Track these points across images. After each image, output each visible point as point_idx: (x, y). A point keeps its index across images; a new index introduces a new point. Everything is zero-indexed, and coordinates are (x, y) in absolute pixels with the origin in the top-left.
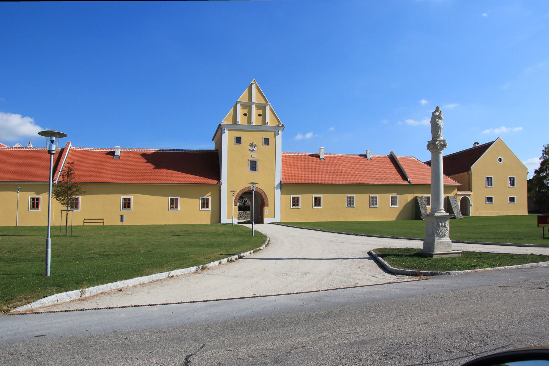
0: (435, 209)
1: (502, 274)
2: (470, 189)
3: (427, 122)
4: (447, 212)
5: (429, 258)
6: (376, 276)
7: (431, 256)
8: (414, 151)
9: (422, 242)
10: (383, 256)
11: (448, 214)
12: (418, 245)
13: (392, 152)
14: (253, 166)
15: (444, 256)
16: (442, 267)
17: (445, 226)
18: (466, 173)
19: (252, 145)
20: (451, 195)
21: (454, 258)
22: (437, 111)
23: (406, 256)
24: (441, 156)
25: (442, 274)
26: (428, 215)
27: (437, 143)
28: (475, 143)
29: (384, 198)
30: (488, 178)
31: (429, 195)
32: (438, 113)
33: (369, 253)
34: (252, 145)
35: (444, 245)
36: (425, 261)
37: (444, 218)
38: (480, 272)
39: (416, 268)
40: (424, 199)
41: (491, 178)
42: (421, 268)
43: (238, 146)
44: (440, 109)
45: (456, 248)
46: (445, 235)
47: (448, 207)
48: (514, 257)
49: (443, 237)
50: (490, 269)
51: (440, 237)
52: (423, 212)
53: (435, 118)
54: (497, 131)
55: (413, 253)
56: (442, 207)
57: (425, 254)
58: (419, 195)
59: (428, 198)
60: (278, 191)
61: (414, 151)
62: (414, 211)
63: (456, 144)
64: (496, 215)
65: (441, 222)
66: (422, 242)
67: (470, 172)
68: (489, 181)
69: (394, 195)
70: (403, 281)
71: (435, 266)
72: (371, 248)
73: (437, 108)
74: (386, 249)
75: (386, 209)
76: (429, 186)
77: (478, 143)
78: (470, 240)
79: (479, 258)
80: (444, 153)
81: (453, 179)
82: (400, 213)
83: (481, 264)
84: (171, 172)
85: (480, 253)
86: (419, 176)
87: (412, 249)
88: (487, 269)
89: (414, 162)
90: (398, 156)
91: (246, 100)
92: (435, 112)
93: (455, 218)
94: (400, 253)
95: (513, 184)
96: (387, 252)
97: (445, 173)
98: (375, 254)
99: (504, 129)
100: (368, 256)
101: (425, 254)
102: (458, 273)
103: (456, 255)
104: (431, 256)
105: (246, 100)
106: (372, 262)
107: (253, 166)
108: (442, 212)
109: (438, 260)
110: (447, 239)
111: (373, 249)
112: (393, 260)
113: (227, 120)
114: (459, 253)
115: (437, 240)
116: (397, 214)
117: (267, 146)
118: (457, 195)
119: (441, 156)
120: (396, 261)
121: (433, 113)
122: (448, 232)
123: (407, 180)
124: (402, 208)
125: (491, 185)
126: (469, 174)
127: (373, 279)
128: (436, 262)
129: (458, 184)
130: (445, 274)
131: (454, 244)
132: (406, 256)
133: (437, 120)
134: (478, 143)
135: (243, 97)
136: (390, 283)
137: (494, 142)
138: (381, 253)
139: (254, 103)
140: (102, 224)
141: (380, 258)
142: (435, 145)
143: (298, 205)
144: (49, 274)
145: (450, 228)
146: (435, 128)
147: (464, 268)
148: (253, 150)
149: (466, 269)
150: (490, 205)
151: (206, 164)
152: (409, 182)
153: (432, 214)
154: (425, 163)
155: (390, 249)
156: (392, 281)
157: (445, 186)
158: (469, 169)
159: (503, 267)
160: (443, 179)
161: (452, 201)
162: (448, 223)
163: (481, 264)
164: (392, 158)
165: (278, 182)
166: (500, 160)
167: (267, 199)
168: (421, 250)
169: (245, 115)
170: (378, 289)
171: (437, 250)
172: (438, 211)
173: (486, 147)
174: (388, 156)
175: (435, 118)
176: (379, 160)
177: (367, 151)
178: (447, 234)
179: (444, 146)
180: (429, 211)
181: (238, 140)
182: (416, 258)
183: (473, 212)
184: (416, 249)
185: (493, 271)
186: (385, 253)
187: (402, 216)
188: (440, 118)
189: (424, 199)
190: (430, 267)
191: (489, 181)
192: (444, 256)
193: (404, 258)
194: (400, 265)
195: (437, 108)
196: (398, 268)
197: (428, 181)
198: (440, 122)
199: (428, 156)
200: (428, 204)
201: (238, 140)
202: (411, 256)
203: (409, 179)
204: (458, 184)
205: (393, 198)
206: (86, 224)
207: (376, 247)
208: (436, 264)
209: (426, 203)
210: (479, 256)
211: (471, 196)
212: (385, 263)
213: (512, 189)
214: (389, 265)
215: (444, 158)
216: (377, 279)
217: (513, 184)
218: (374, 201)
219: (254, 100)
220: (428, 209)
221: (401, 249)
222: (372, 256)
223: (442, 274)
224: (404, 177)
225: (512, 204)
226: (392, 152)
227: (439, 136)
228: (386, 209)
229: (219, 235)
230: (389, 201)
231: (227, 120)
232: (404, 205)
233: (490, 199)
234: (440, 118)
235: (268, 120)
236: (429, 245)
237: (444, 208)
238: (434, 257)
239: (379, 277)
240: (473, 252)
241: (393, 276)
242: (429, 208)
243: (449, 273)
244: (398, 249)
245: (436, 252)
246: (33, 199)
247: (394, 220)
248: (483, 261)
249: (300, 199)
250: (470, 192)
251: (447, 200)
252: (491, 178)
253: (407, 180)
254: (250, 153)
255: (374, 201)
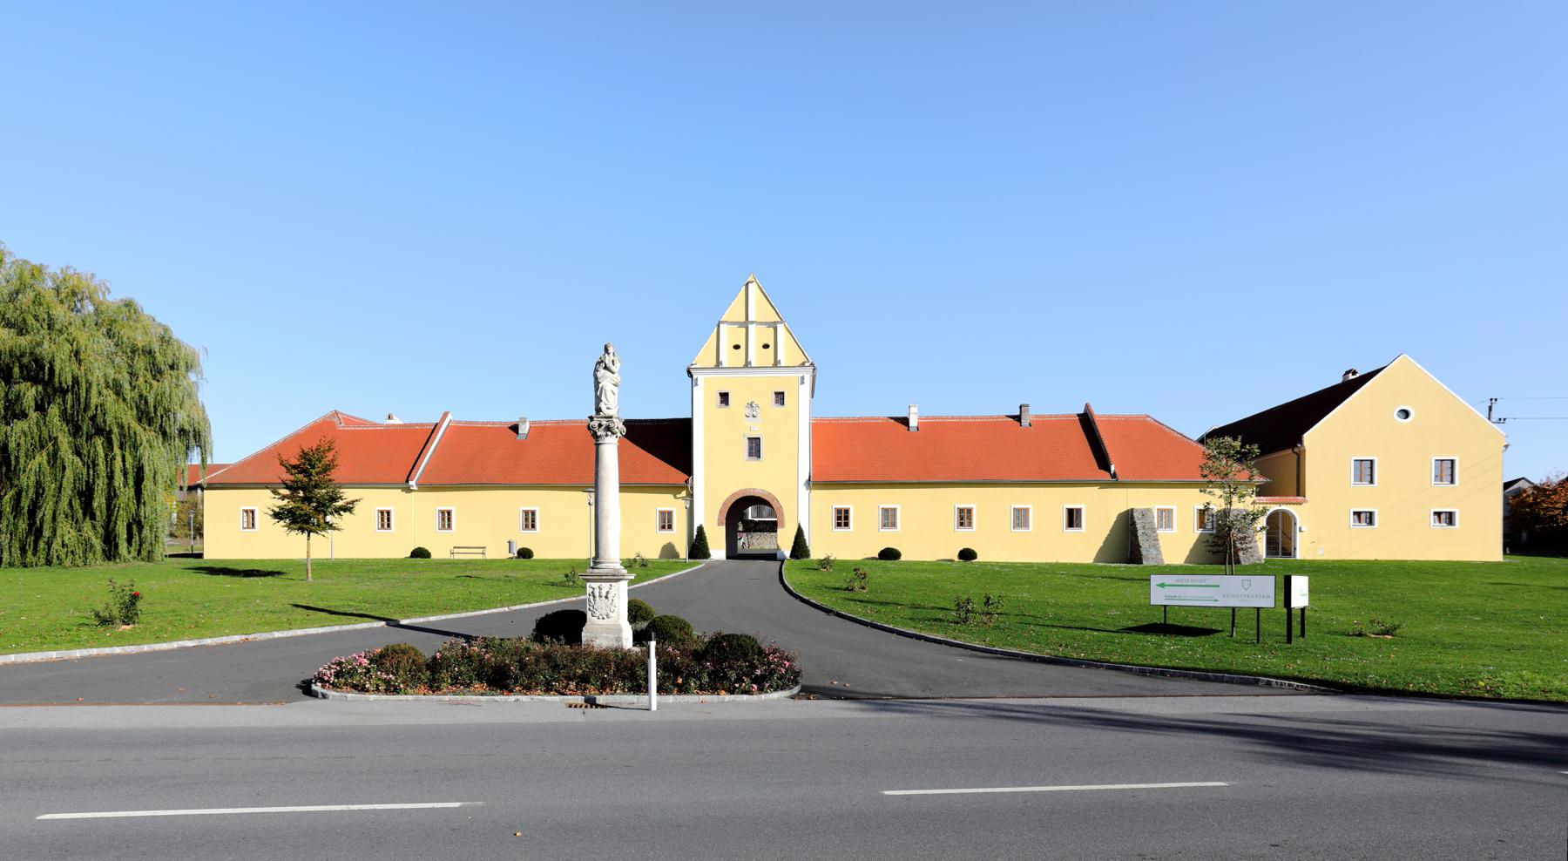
14: (755, 447)
43: (724, 409)
68: (1366, 470)
77: (1354, 373)
84: (38, 708)
90: (1098, 412)
107: (755, 447)
113: (705, 357)
135: (735, 311)
140: (480, 557)
143: (847, 525)
151: (666, 442)
158: (1300, 441)
164: (1086, 420)
176: (1050, 426)
191: (1366, 470)
203: (1113, 468)
206: (457, 557)
231: (705, 357)
249: (974, 513)
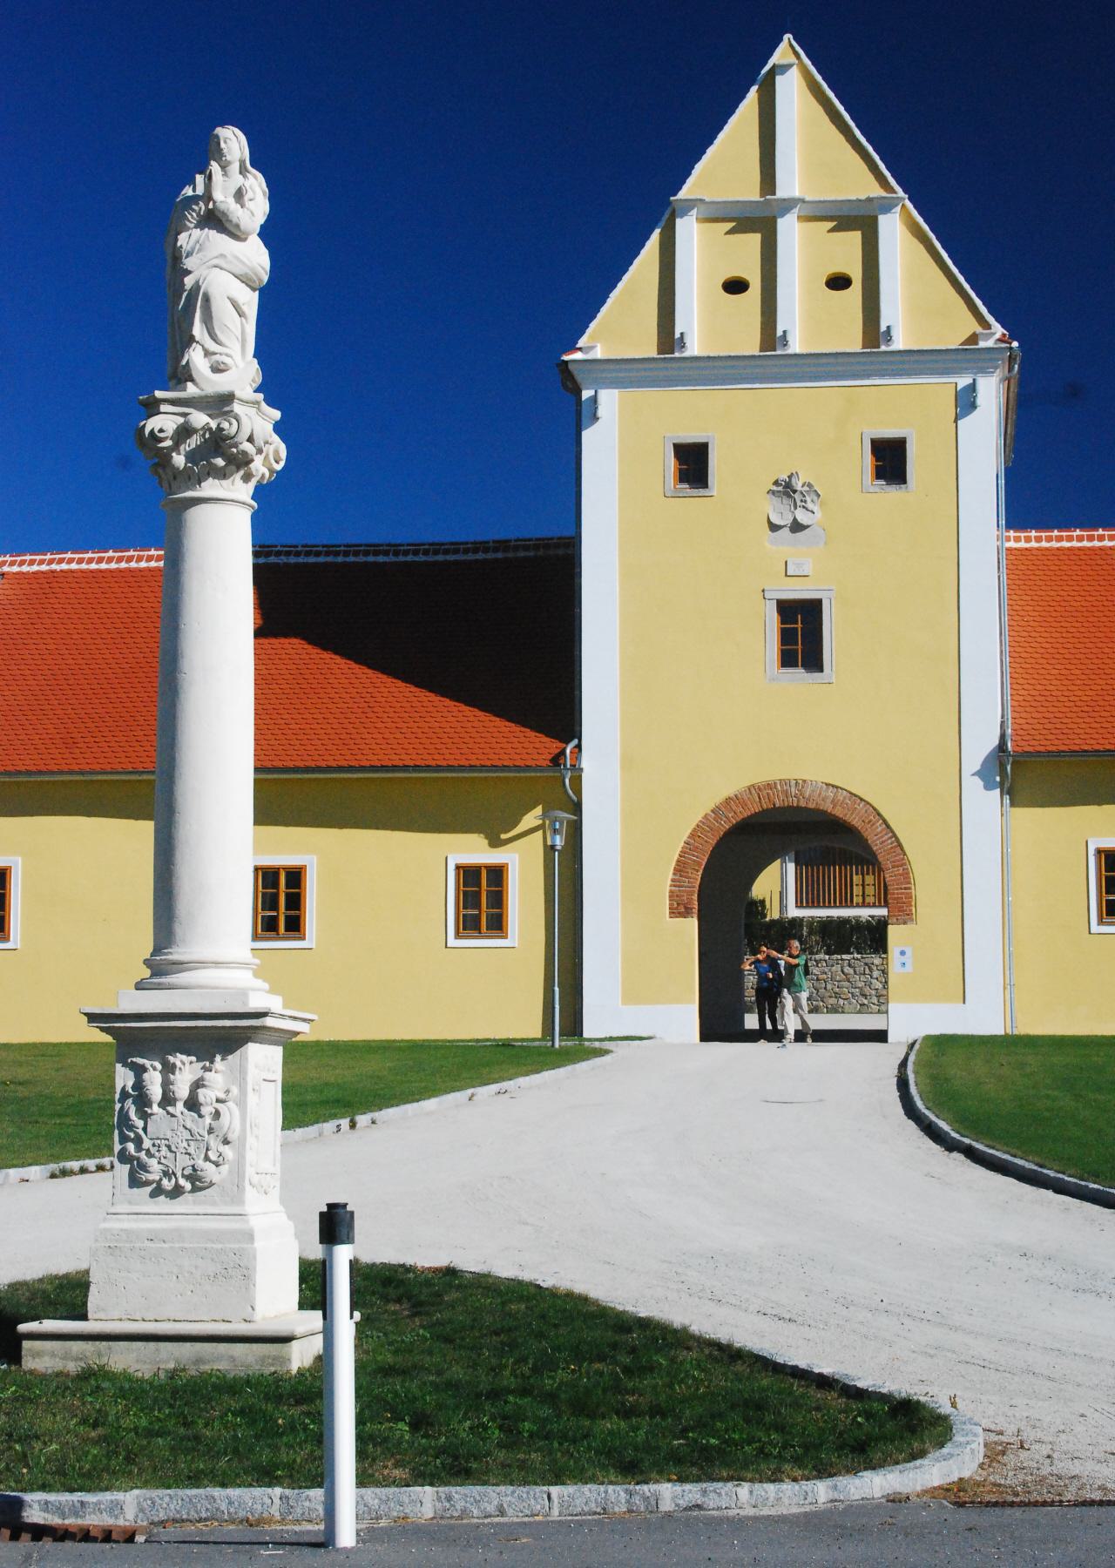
14: (801, 634)
19: (786, 490)
34: (786, 490)
43: (692, 505)
60: (984, 804)
91: (749, 191)
105: (749, 191)
107: (801, 634)
117: (893, 493)
139: (788, 205)
144: (346, 1536)
148: (797, 527)
165: (982, 737)
167: (689, 849)
169: (735, 286)
181: (693, 464)
201: (693, 464)
219: (790, 184)
229: (20, 1084)
235: (892, 313)
246: (469, 875)
254: (784, 547)
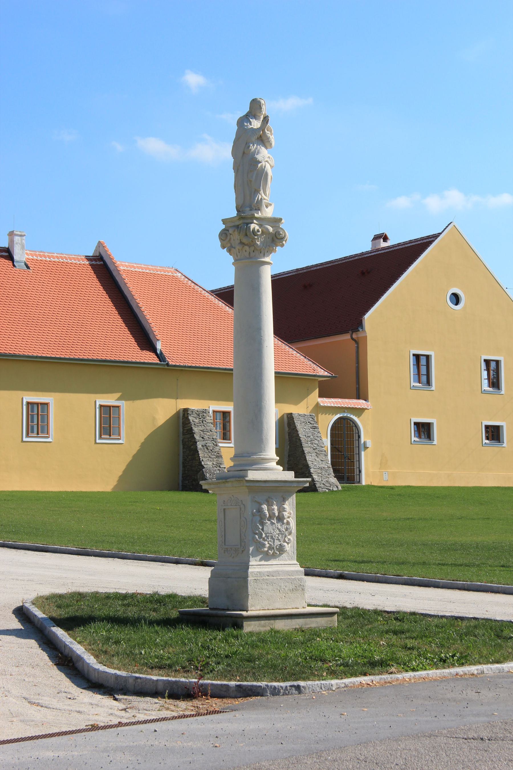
0: (247, 458)
1: (471, 694)
2: (360, 393)
3: (218, 154)
4: (288, 468)
5: (229, 630)
6: (45, 700)
7: (237, 623)
8: (179, 252)
9: (206, 573)
10: (70, 623)
11: (290, 475)
12: (191, 582)
13: (100, 244)
15: (280, 625)
16: (274, 667)
17: (280, 519)
18: (347, 337)
20: (299, 410)
21: (315, 633)
22: (255, 117)
23: (151, 623)
24: (267, 275)
25: (275, 692)
26: (224, 479)
27: (254, 226)
28: (377, 238)
29: (72, 410)
30: (417, 357)
31: (228, 407)
32: (256, 124)
33: (21, 613)
35: (282, 586)
36: (217, 640)
37: (275, 491)
38: (402, 683)
39: (185, 670)
40: (210, 419)
41: (428, 357)
42: (204, 669)
44: (265, 110)
45: (321, 597)
46: (281, 549)
47: (292, 454)
48: (506, 633)
49: (274, 556)
50: (433, 673)
51: (267, 557)
52: (207, 463)
53: (249, 139)
54: (433, 203)
55: (174, 614)
56: (271, 451)
57: (216, 616)
58: (194, 405)
59: (225, 415)
61: (179, 252)
62: (179, 461)
63: (316, 237)
64: (446, 484)
65: (270, 505)
66: (206, 573)
67: (360, 334)
68: (422, 364)
69: (109, 400)
70: (141, 717)
71: (250, 660)
72: (25, 594)
73: (255, 106)
74: (81, 596)
75: (83, 450)
76: (227, 373)
78: (366, 569)
79: (395, 633)
80: (278, 263)
81: (307, 354)
82: (130, 466)
83: (401, 654)
85: (399, 616)
86: (192, 336)
87: (172, 597)
88: (423, 673)
89: (175, 287)
90: (124, 261)
92: (247, 118)
93: (312, 488)
94: (132, 612)
95: (495, 383)
96: (83, 609)
97: (278, 332)
98: (39, 614)
99: (455, 197)
100: (16, 624)
101: (216, 616)
102: (329, 688)
103: (322, 622)
104: (237, 623)
106: (32, 644)
108: (272, 469)
109: (262, 640)
110: (289, 564)
111: (33, 596)
112: (108, 639)
114: (331, 614)
115: (256, 567)
116: (119, 467)
118: (318, 409)
119: (267, 275)
120: (117, 642)
121: (242, 121)
122: (293, 538)
123: (152, 348)
124: (135, 448)
125: (428, 383)
126: (356, 341)
127: (33, 712)
128: (254, 646)
129: (321, 372)
130: (286, 692)
131: (312, 582)
132: (151, 623)
133: (253, 148)
134: (386, 239)
136: (94, 728)
137: (436, 236)
138: (62, 613)
141: (59, 632)
142: (246, 234)
145: (298, 524)
146: (249, 177)
147: (348, 669)
149: (354, 674)
150: (423, 448)
152: (161, 357)
153: (236, 476)
154: (213, 292)
155: (96, 596)
156: (102, 720)
157: (279, 376)
158: (356, 324)
159: (474, 669)
160: (274, 354)
161: (303, 430)
162: (290, 507)
163: (401, 654)
164: (101, 267)
166: (456, 299)
168: (202, 601)
170: (50, 754)
171: (260, 601)
172: (257, 463)
173: (411, 252)
174: (88, 258)
175: (249, 139)
176: (56, 270)
177: (11, 234)
178: (287, 547)
179: (276, 239)
180: (227, 463)
182: (186, 632)
183: (371, 471)
184: (185, 599)
185: (443, 679)
186: (78, 613)
187: (135, 477)
188: (262, 139)
189: (210, 419)
190: (249, 664)
191: (422, 364)
192: (280, 625)
193: (146, 632)
194: (131, 658)
195: (255, 106)
196: (124, 667)
197: (223, 355)
198: (263, 155)
199: (223, 271)
200: (226, 437)
202: (168, 623)
203: (159, 346)
204: (321, 372)
205: (106, 409)
207: (46, 591)
208: (256, 653)
209: (217, 432)
210: (396, 625)
211: (365, 414)
212: (79, 649)
213: (494, 399)
214: (90, 659)
215: (279, 282)
216: (49, 715)
217: (495, 383)
218: (37, 419)
220: (223, 452)
221: (133, 596)
222: (28, 624)
223: (275, 692)
224: (145, 339)
225: (492, 450)
226: (100, 244)
227: (260, 202)
228: (83, 450)
230: (92, 421)
232: (142, 438)
233: (424, 430)
234: (262, 139)
236: (231, 584)
237: (278, 452)
238: (249, 627)
239: (54, 703)
240: (377, 612)
241: (106, 701)
242: (227, 449)
243: (298, 688)
244: (125, 597)
245: (254, 608)
247: (108, 488)
248: (410, 643)
250: (360, 403)
251: (288, 427)
252: (428, 357)
253: (152, 348)
255: (37, 419)
